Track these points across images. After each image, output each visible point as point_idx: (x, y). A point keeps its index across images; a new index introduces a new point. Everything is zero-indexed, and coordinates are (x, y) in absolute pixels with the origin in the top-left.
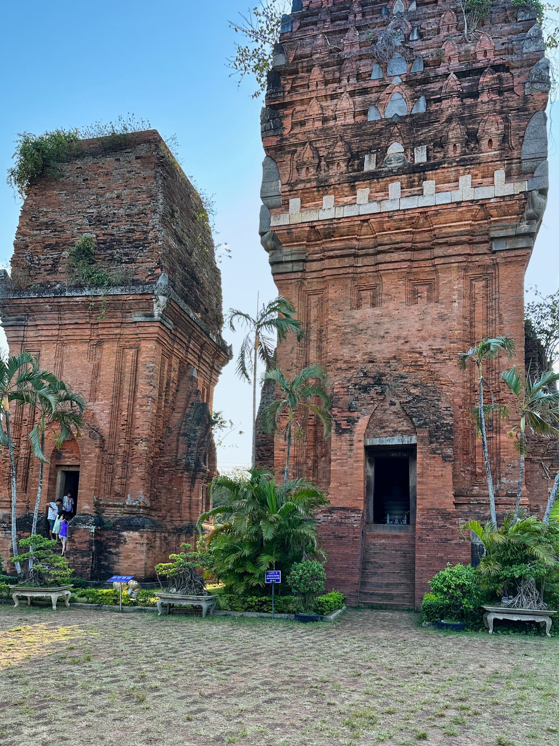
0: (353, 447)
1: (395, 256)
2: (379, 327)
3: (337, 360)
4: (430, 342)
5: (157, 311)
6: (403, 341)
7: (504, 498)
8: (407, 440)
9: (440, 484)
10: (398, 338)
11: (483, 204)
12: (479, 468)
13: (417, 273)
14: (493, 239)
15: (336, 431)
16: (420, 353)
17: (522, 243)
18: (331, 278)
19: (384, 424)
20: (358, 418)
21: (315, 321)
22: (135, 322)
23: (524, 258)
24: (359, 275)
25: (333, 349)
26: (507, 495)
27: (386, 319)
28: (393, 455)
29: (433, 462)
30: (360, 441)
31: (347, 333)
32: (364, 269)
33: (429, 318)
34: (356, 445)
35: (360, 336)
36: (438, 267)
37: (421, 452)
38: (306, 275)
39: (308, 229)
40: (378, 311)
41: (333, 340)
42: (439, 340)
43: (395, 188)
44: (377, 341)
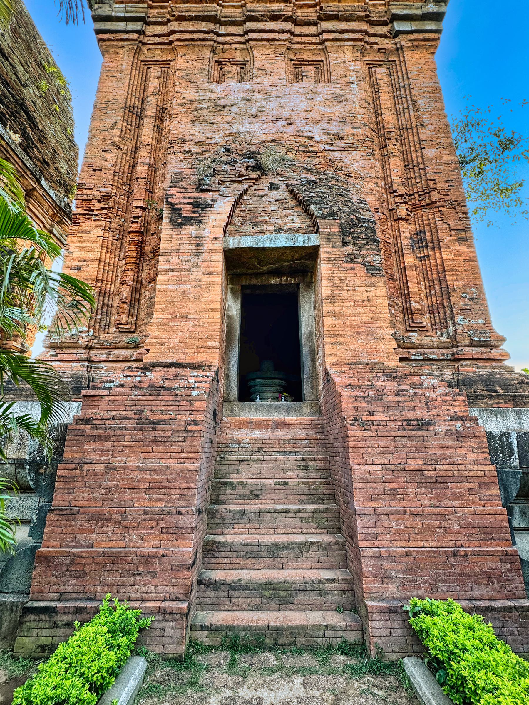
0: (202, 249)
2: (249, 104)
3: (184, 141)
4: (324, 124)
6: (285, 123)
7: (469, 350)
8: (301, 240)
9: (366, 316)
10: (278, 118)
12: (416, 301)
15: (172, 220)
16: (311, 138)
17: (430, 26)
18: (182, 43)
19: (260, 219)
20: (214, 200)
21: (154, 94)
23: (434, 43)
25: (179, 125)
26: (472, 344)
27: (259, 96)
28: (273, 282)
29: (350, 275)
30: (216, 239)
31: (201, 109)
34: (208, 244)
35: (221, 113)
36: (327, 43)
37: (329, 259)
40: (247, 86)
41: (180, 116)
42: (335, 123)
44: (246, 120)
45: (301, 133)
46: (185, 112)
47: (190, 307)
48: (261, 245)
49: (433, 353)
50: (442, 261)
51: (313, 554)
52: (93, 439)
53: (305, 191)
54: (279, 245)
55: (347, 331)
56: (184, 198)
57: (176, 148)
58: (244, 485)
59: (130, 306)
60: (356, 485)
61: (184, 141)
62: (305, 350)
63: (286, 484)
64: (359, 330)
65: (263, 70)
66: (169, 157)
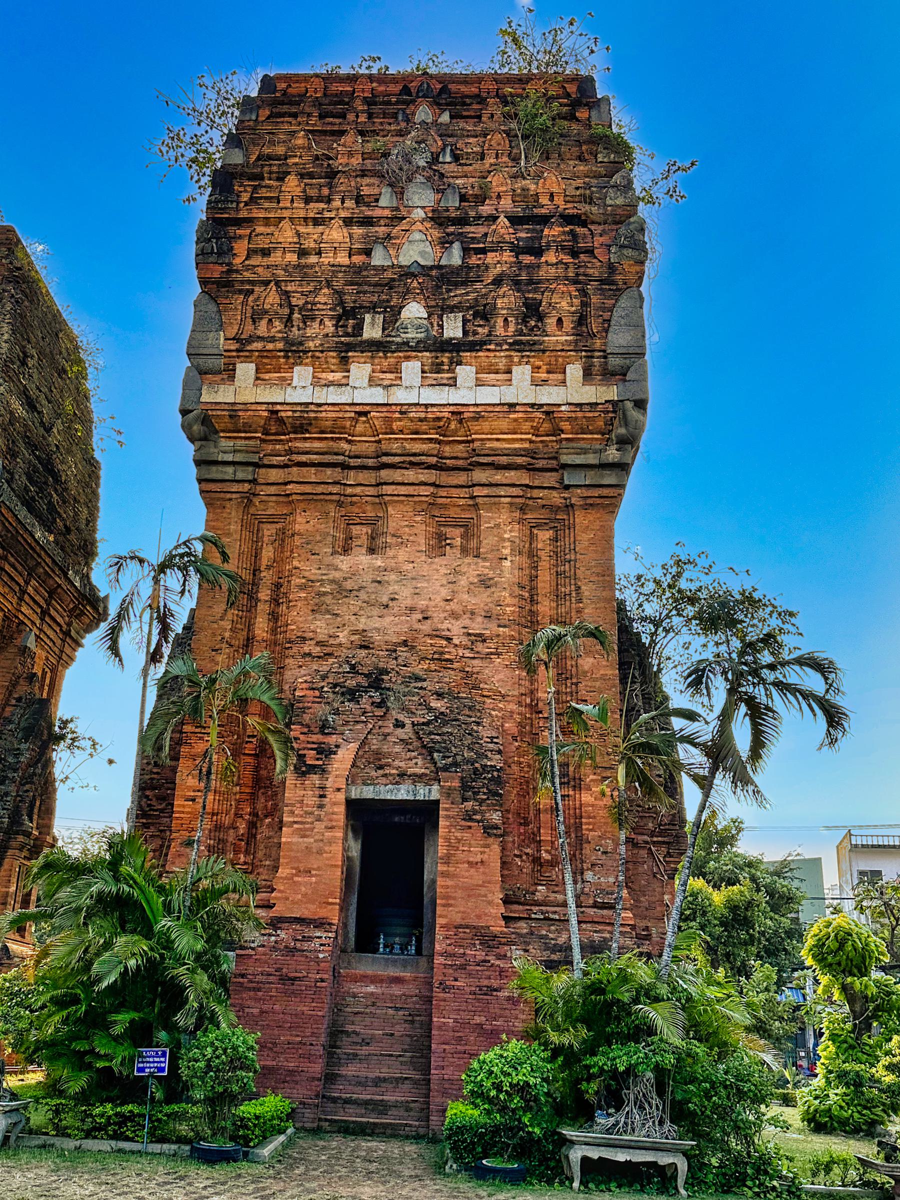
1: (411, 475)
3: (304, 639)
6: (420, 616)
8: (423, 793)
10: (412, 609)
13: (444, 506)
14: (564, 466)
16: (449, 639)
18: (301, 498)
19: (384, 761)
20: (337, 746)
21: (268, 567)
23: (613, 501)
24: (349, 499)
26: (595, 905)
27: (393, 577)
28: (396, 819)
29: (467, 835)
30: (339, 790)
31: (325, 594)
32: (358, 490)
33: (463, 581)
34: (331, 796)
37: (448, 817)
41: (299, 604)
42: (480, 619)
44: (376, 611)
45: (438, 633)
46: (306, 599)
47: (314, 862)
48: (382, 797)
49: (555, 912)
50: (581, 805)
51: (407, 1086)
52: (249, 989)
53: (431, 733)
54: (400, 797)
55: (459, 893)
56: (308, 742)
57: (295, 650)
58: (357, 1034)
59: (247, 844)
60: (433, 1032)
61: (304, 639)
62: (426, 900)
63: (392, 1035)
64: (471, 891)
65: (398, 537)
66: (287, 661)
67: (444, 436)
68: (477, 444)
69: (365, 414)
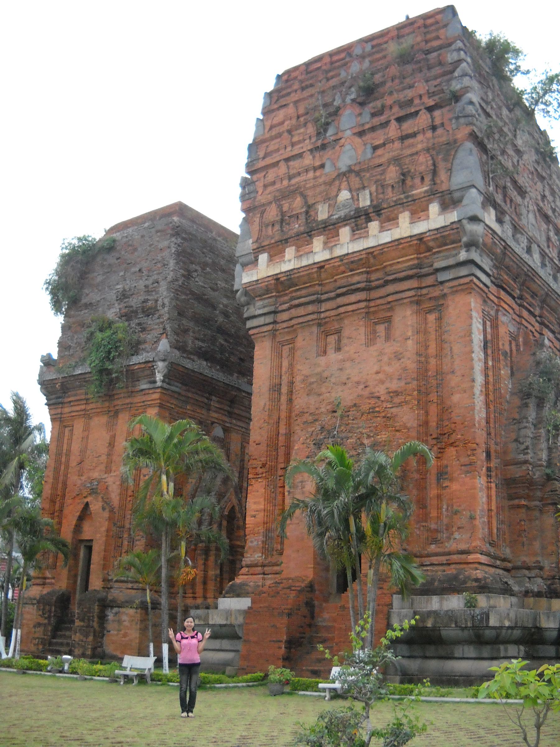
1: (353, 298)
4: (388, 385)
5: (159, 377)
10: (358, 383)
11: (420, 238)
13: (375, 313)
14: (437, 270)
16: (379, 398)
18: (299, 326)
22: (142, 390)
24: (324, 321)
31: (313, 383)
32: (327, 314)
33: (385, 359)
38: (278, 325)
39: (273, 282)
42: (395, 381)
43: (345, 232)
67: (369, 268)
68: (388, 269)
69: (322, 267)
